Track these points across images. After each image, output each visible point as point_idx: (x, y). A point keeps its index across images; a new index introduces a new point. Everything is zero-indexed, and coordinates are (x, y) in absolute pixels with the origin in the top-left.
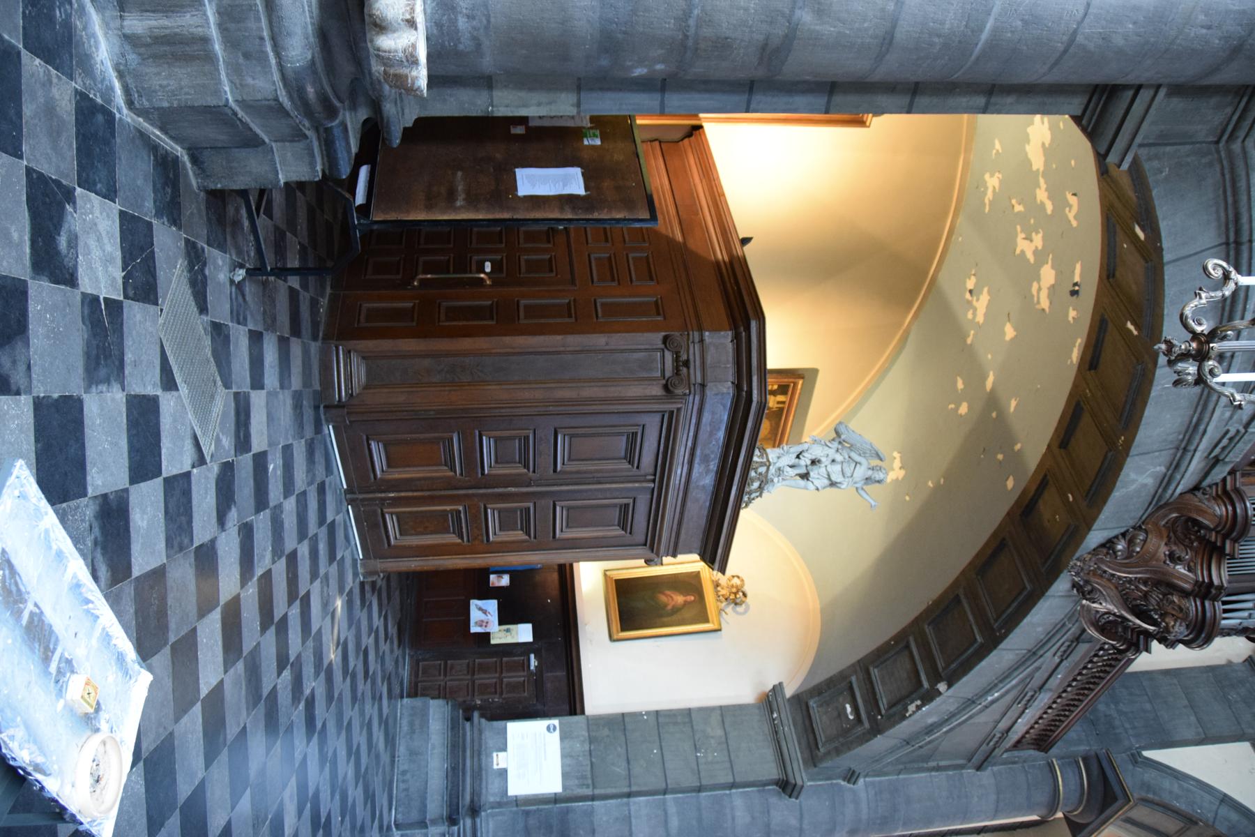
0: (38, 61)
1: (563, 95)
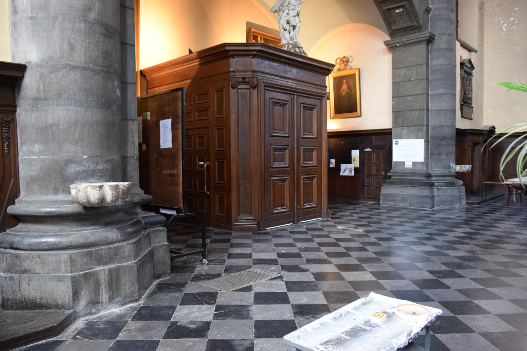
0: (120, 334)
1: (129, 126)
